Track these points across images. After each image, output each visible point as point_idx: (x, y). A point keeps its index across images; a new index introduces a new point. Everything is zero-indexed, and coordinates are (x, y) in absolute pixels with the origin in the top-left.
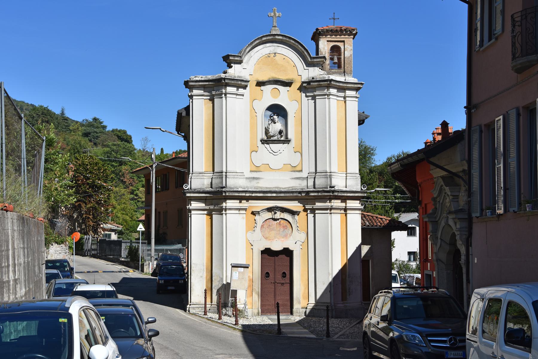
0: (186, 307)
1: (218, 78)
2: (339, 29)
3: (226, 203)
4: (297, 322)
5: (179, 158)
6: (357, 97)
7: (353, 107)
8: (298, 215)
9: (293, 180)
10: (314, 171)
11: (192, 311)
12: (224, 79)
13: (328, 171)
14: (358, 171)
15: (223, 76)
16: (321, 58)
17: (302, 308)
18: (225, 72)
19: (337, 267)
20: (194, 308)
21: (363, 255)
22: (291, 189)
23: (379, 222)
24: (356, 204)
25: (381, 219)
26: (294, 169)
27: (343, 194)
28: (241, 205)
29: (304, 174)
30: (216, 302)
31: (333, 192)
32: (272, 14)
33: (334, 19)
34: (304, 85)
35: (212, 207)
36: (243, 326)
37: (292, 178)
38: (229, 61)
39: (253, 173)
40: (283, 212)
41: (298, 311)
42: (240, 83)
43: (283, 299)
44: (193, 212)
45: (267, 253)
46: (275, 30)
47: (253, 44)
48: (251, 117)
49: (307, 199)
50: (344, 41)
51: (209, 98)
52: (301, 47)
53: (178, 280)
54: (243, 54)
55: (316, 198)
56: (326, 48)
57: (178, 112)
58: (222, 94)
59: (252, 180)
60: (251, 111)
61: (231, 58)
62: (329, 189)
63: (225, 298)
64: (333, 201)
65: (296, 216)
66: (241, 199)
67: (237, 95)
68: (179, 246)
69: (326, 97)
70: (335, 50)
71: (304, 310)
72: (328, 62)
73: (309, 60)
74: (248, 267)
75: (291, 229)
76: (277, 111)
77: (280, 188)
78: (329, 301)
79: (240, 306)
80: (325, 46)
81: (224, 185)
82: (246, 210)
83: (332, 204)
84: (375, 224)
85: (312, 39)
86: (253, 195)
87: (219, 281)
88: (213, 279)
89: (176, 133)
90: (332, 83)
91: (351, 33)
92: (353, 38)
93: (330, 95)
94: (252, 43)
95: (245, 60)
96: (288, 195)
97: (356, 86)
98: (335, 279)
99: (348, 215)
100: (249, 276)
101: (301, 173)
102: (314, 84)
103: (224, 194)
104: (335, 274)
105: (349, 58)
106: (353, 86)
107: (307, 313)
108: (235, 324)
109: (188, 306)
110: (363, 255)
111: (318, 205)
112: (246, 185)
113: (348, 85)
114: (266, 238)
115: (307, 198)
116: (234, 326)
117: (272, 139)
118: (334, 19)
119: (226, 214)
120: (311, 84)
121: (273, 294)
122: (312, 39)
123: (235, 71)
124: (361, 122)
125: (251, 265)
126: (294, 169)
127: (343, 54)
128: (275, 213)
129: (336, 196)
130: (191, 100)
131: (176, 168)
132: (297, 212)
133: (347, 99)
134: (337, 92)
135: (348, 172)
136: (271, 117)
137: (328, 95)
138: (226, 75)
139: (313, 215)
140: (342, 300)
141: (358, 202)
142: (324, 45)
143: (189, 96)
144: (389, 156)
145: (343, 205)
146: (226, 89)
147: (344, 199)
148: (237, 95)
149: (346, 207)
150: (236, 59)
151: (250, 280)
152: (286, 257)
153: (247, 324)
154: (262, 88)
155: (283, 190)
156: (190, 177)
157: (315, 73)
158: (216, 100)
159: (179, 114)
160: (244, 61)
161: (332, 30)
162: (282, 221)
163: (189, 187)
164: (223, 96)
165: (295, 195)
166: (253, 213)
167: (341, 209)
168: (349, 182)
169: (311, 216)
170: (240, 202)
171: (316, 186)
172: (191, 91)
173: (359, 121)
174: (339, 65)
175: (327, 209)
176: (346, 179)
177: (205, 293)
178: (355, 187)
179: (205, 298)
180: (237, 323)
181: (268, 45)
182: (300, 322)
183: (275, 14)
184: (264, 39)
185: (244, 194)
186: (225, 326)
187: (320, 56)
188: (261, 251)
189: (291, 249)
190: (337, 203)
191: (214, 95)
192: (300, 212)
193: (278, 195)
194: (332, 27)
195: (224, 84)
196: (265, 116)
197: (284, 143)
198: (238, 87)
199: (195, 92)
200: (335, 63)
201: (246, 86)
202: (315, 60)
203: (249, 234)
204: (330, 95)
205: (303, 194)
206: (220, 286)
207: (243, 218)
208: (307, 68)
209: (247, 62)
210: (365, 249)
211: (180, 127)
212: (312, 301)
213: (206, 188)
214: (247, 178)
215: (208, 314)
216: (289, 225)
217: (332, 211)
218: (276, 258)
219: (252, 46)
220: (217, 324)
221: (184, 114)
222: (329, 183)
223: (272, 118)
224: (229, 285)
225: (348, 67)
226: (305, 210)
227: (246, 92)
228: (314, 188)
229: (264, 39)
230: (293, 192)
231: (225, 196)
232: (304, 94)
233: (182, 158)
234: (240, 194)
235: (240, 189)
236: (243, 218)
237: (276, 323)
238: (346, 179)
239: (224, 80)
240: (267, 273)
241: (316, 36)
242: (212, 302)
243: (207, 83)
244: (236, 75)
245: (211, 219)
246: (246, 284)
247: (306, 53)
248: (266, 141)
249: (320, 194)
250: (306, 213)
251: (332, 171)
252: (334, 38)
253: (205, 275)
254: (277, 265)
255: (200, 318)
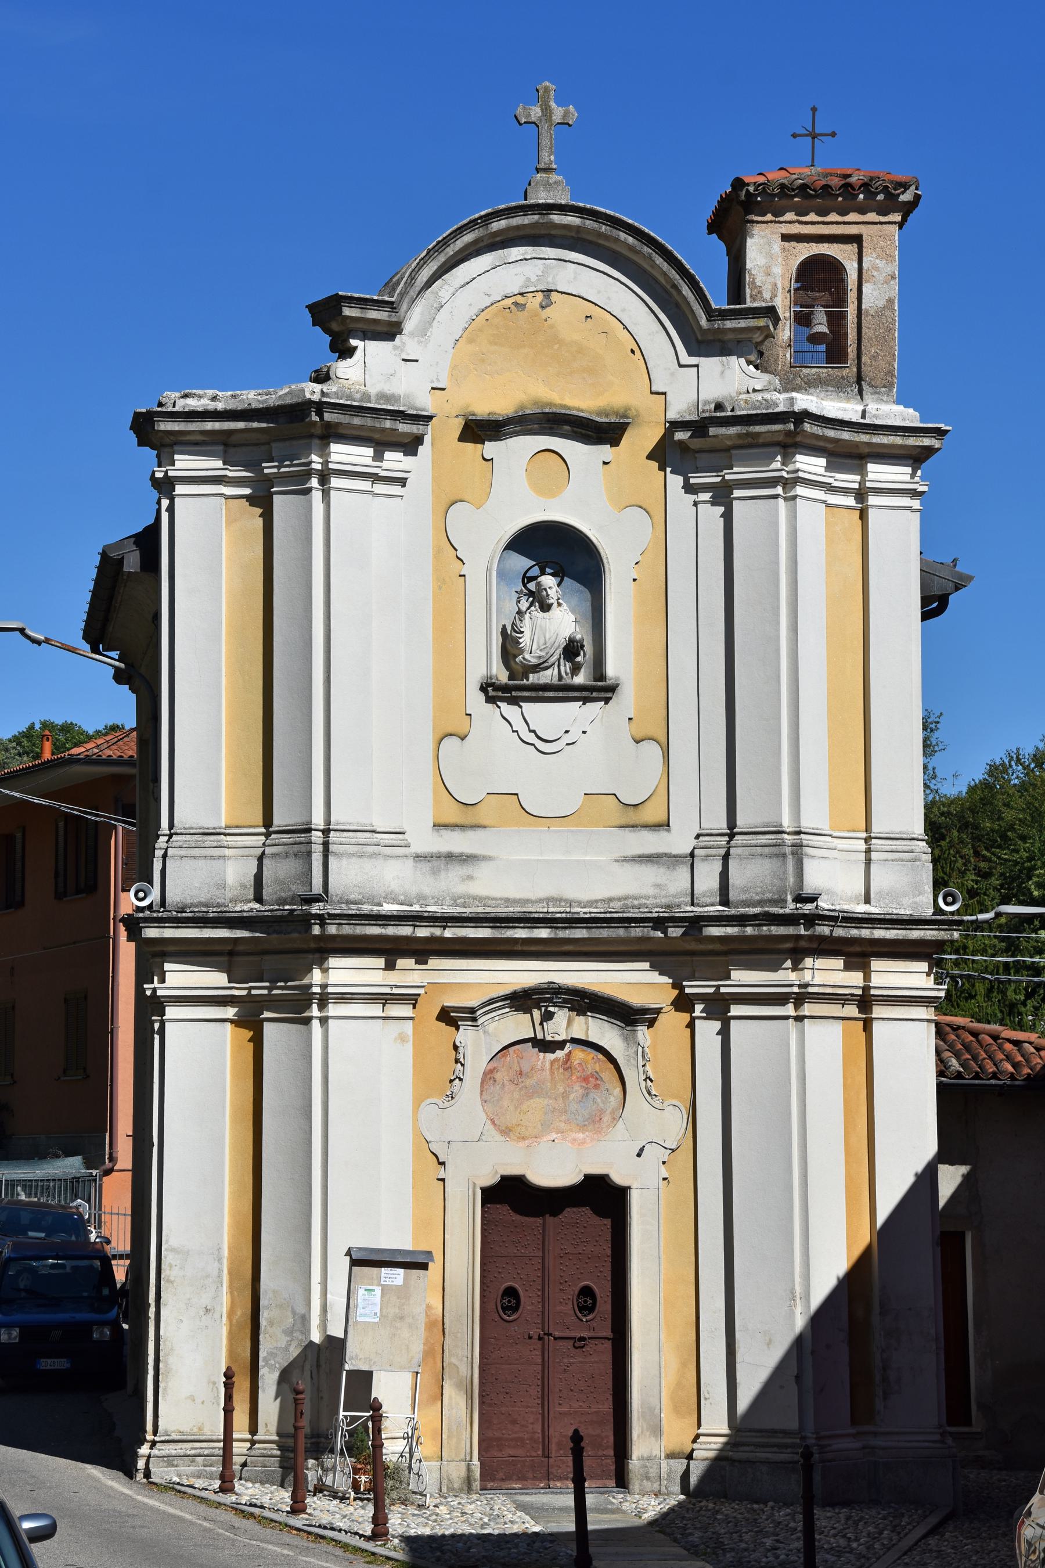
0: (135, 1456)
1: (289, 401)
2: (835, 182)
3: (325, 971)
4: (652, 1523)
5: (73, 760)
6: (915, 494)
7: (898, 537)
8: (651, 1023)
9: (627, 866)
10: (722, 825)
11: (161, 1473)
12: (320, 407)
13: (787, 824)
14: (918, 827)
15: (312, 391)
16: (755, 312)
17: (671, 1456)
18: (322, 377)
19: (829, 1265)
20: (169, 1460)
21: (942, 1203)
22: (617, 905)
23: (1008, 1058)
24: (913, 976)
25: (1017, 1043)
26: (632, 817)
27: (854, 932)
28: (393, 978)
29: (679, 840)
30: (273, 1427)
31: (811, 920)
32: (536, 112)
33: (814, 136)
34: (680, 436)
35: (260, 988)
36: (410, 1541)
37: (625, 859)
38: (338, 325)
39: (446, 833)
40: (581, 1012)
41: (653, 1472)
42: (388, 424)
43: (581, 1409)
44: (171, 1012)
45: (510, 1198)
46: (548, 186)
47: (450, 251)
48: (440, 581)
49: (692, 953)
50: (857, 240)
51: (247, 491)
52: (665, 266)
53: (86, 1328)
54: (402, 295)
55: (733, 946)
56: (778, 270)
57: (104, 555)
58: (308, 474)
59: (441, 864)
60: (438, 553)
61: (347, 312)
62: (790, 907)
63: (319, 1408)
64: (808, 962)
65: (643, 1033)
66: (391, 951)
67: (375, 478)
68: (71, 1166)
69: (779, 490)
70: (820, 279)
71: (680, 1465)
72: (785, 332)
73: (703, 322)
74: (424, 1266)
75: (618, 1090)
76: (557, 552)
77: (570, 903)
78: (794, 1425)
79: (393, 1449)
80: (771, 259)
81: (317, 888)
82: (413, 1000)
83: (807, 976)
84: (991, 1068)
85: (714, 227)
86: (448, 933)
87: (289, 1332)
88: (263, 1322)
89: (86, 647)
90: (807, 427)
91: (888, 198)
92: (901, 225)
93: (797, 481)
94: (445, 243)
95: (413, 319)
96: (604, 933)
97: (912, 441)
98: (819, 1319)
99: (876, 1025)
100: (429, 1307)
101: (663, 834)
102: (723, 431)
103: (316, 930)
104: (819, 1295)
105: (879, 314)
106: (898, 440)
107: (694, 1479)
108: (374, 1536)
109: (144, 1450)
110: (942, 1203)
111: (743, 978)
112: (413, 890)
113: (876, 439)
114: (506, 1131)
115: (693, 946)
116: (369, 1546)
117: (533, 679)
118: (814, 136)
119: (324, 1021)
120: (712, 431)
121: (535, 1391)
122: (714, 227)
123: (368, 372)
124: (934, 604)
125: (438, 1256)
126: (632, 817)
127: (852, 296)
128: (548, 1016)
129: (822, 939)
130: (165, 503)
131: (65, 808)
132: (645, 1011)
133: (873, 500)
134: (828, 468)
135: (876, 829)
136: (527, 579)
137: (789, 483)
138: (325, 387)
139: (717, 1025)
140: (854, 1422)
141: (924, 966)
142: (770, 256)
143: (155, 482)
144: (998, 756)
145: (856, 978)
146: (324, 453)
147: (858, 955)
148: (375, 478)
149: (866, 989)
150: (373, 314)
151: (430, 1325)
152: (596, 1220)
153: (427, 1531)
154: (490, 448)
155: (582, 912)
156: (159, 853)
157: (730, 381)
158: (279, 502)
159: (109, 566)
160: (408, 327)
161: (804, 187)
162: (580, 1054)
163: (155, 895)
164: (314, 482)
165: (637, 932)
166: (448, 1017)
167: (842, 999)
168: (883, 878)
169: (708, 1030)
170: (390, 966)
171: (733, 896)
172: (165, 458)
173: (925, 600)
174: (832, 348)
175: (780, 999)
176: (868, 862)
177: (229, 1386)
178: (906, 901)
179: (228, 1411)
180: (380, 1532)
181: (515, 252)
182: (663, 1524)
183: (547, 111)
184: (497, 225)
185: (405, 931)
186: (323, 1546)
187: (749, 304)
188: (485, 1191)
189: (619, 1178)
190: (827, 973)
191: (269, 481)
192: (658, 1011)
193: (562, 934)
194: (803, 172)
195: (318, 431)
196: (502, 575)
197: (585, 700)
198: (382, 444)
199: (185, 463)
200: (815, 339)
201: (418, 440)
202: (729, 324)
203: (429, 1110)
204: (797, 481)
205: (675, 932)
206: (294, 1352)
207: (402, 1038)
208: (694, 360)
209: (423, 332)
210: (950, 1180)
211: (106, 620)
212: (717, 1423)
213: (235, 901)
214: (418, 857)
215: (238, 1486)
216: (608, 1073)
217: (808, 1009)
218: (550, 1220)
219: (442, 258)
220: (287, 1537)
221: (132, 563)
222: (791, 880)
223: (532, 586)
224: (335, 1347)
225: (874, 357)
226: (683, 1003)
227: (414, 467)
228: (725, 901)
229: (497, 225)
230: (626, 922)
231: (323, 937)
232: (679, 480)
233: (88, 761)
234: (391, 931)
235: (389, 908)
236: (402, 1038)
237: (572, 1527)
238: (868, 862)
239: (320, 414)
240: (511, 1293)
241: (733, 217)
242: (253, 1429)
243: (241, 425)
244: (373, 390)
245: (257, 1042)
246: (416, 1345)
247: (686, 291)
248: (505, 688)
249: (749, 930)
250: (685, 1017)
251: (806, 824)
252: (813, 224)
253: (223, 1299)
254: (554, 1254)
255: (202, 1508)
